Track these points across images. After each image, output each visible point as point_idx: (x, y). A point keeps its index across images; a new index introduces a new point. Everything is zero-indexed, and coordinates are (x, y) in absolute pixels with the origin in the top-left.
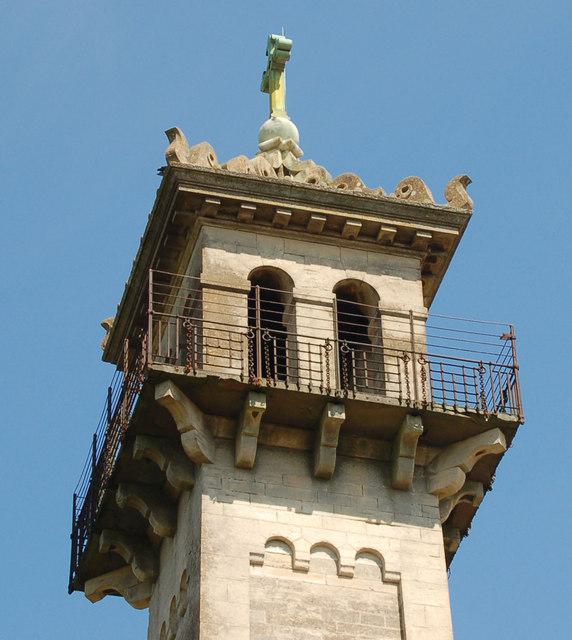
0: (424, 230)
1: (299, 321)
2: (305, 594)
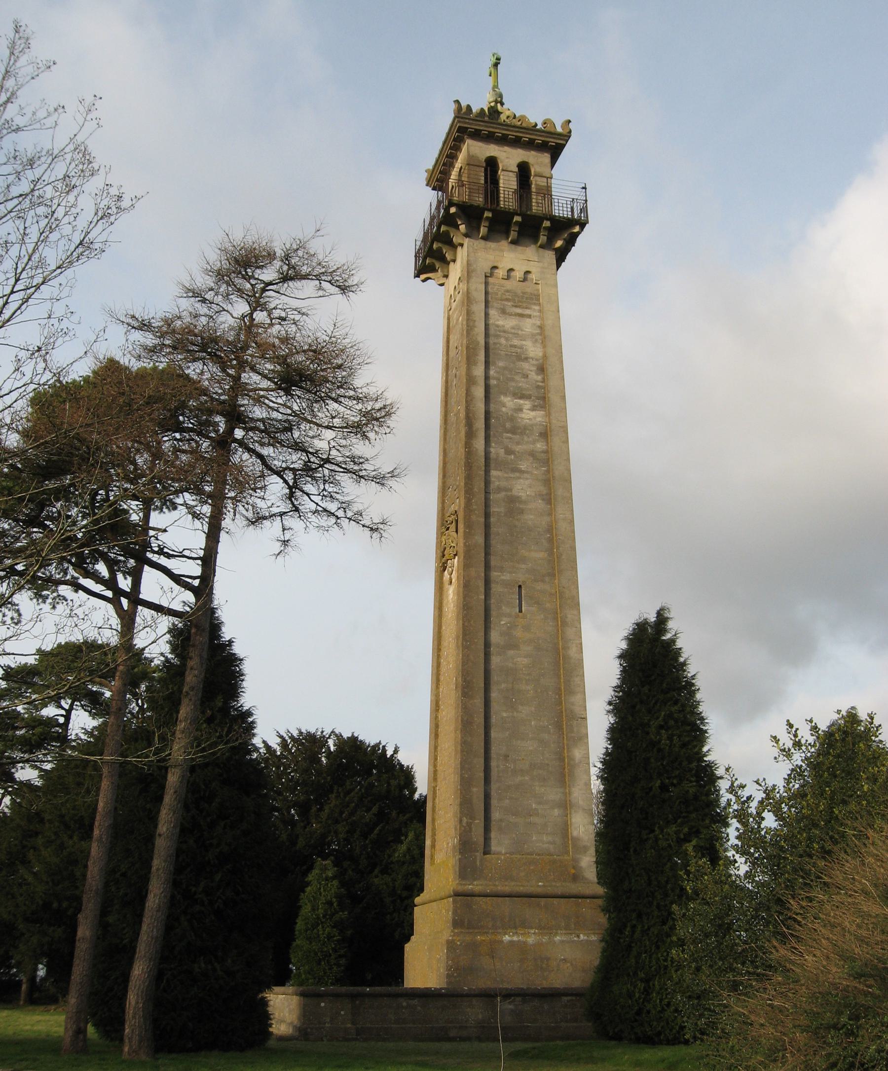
0: (552, 142)
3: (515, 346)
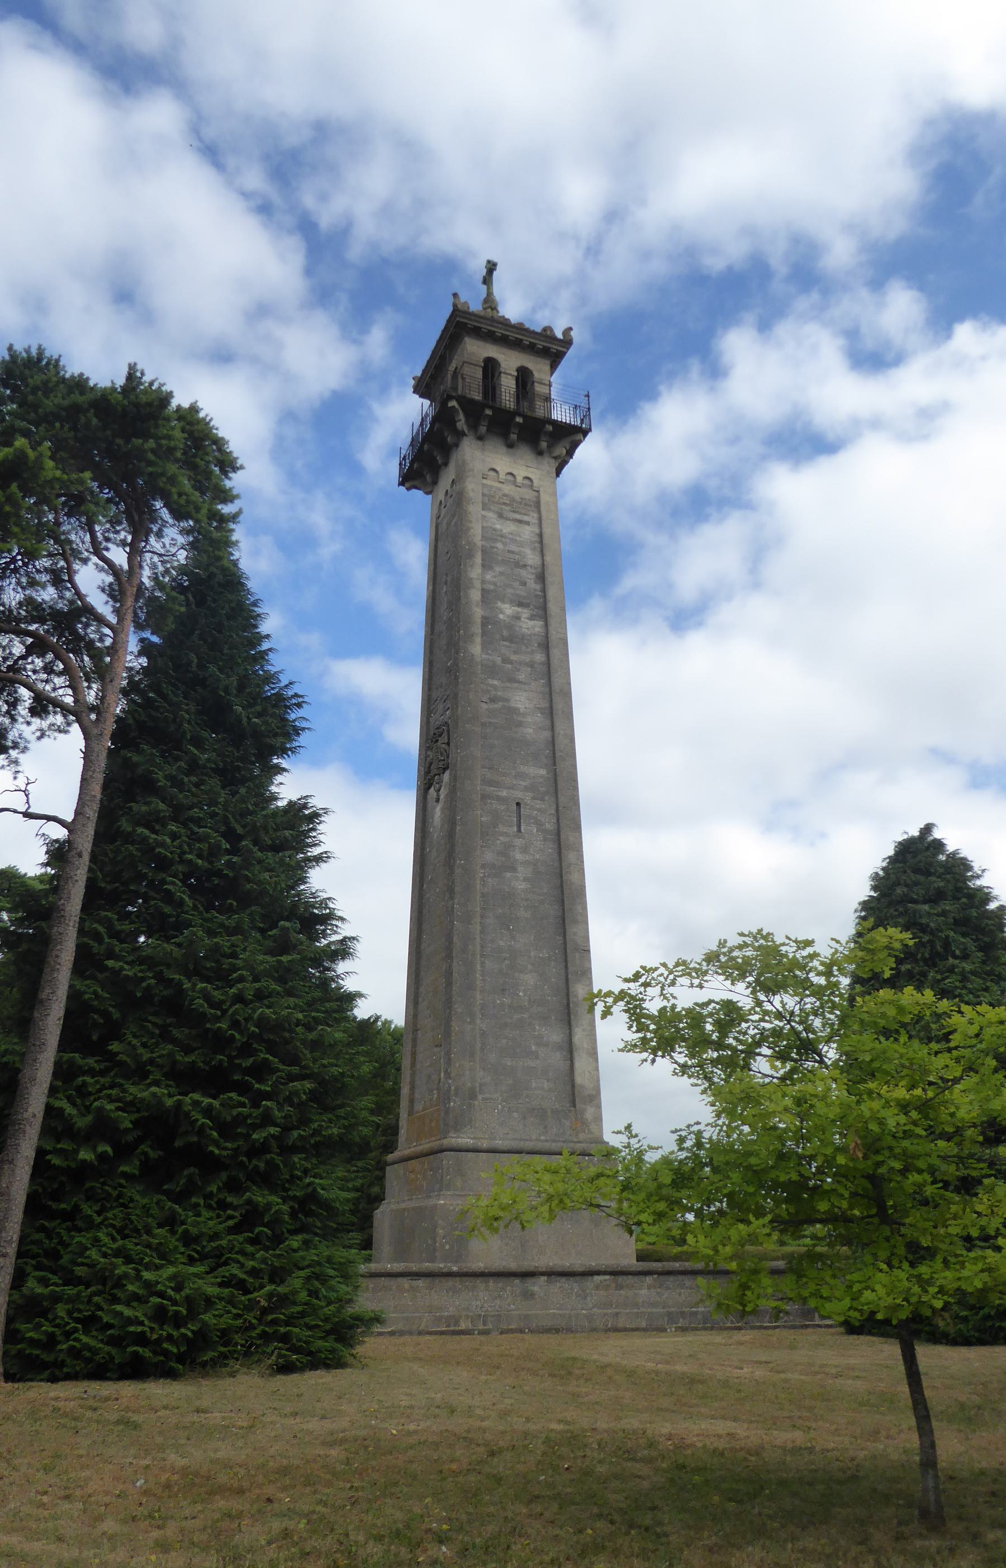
3: (513, 552)
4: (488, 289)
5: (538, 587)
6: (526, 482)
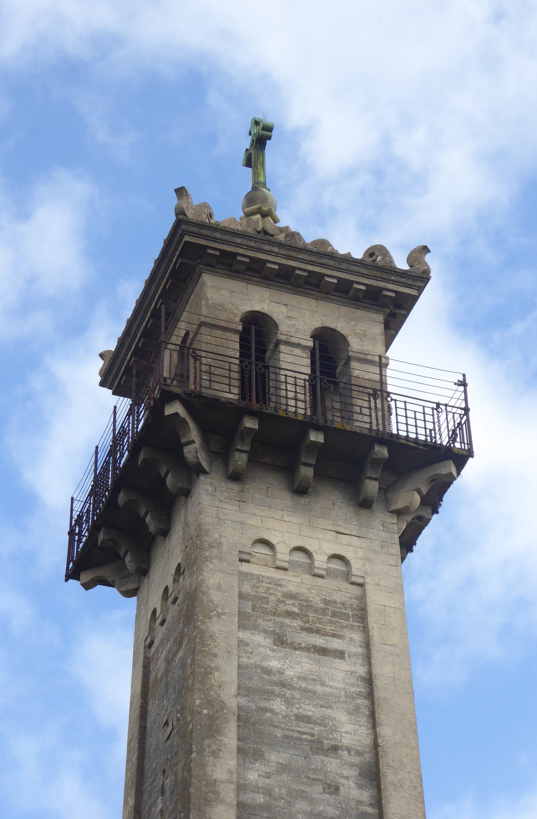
1: (238, 347)
2: (284, 589)
3: (307, 719)
4: (256, 175)
5: (365, 795)
6: (336, 565)
